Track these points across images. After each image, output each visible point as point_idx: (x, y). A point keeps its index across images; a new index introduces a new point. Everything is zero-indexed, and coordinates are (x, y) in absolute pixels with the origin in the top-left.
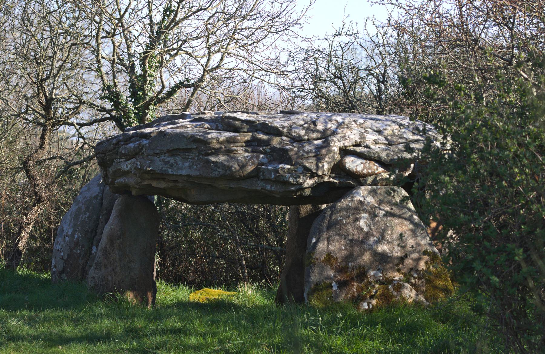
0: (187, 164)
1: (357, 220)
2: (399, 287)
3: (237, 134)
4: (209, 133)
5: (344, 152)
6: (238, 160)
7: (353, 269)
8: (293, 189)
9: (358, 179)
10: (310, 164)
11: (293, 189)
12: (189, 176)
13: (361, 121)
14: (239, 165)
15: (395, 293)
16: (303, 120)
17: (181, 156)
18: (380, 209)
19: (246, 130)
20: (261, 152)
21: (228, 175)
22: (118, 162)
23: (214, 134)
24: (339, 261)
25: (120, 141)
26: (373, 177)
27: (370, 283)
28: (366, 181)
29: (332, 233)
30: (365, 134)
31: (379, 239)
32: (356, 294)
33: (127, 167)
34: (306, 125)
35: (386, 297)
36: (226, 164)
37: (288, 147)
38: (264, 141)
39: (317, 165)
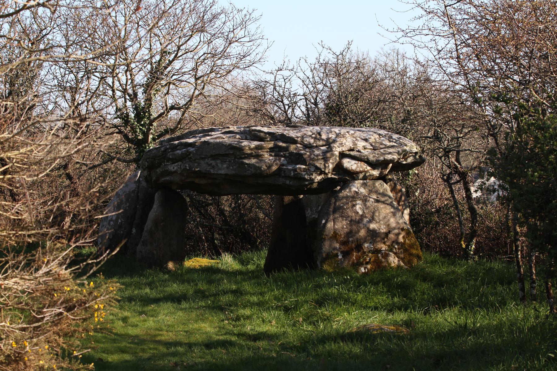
0: (225, 166)
1: (354, 206)
2: (386, 256)
3: (263, 143)
4: (242, 142)
5: (343, 155)
6: (265, 162)
7: (352, 243)
8: (307, 183)
9: (353, 175)
10: (320, 164)
11: (307, 183)
12: (226, 175)
13: (352, 132)
14: (266, 166)
15: (383, 260)
16: (311, 132)
17: (220, 159)
18: (370, 198)
19: (268, 139)
20: (282, 156)
21: (258, 174)
22: (165, 165)
23: (245, 143)
24: (343, 236)
25: (168, 149)
26: (363, 173)
27: (364, 253)
28: (358, 177)
29: (337, 215)
30: (356, 142)
31: (370, 220)
32: (355, 261)
33: (174, 168)
34: (314, 136)
35: (377, 263)
36: (257, 165)
37: (302, 152)
38: (284, 147)
39: (325, 165)
